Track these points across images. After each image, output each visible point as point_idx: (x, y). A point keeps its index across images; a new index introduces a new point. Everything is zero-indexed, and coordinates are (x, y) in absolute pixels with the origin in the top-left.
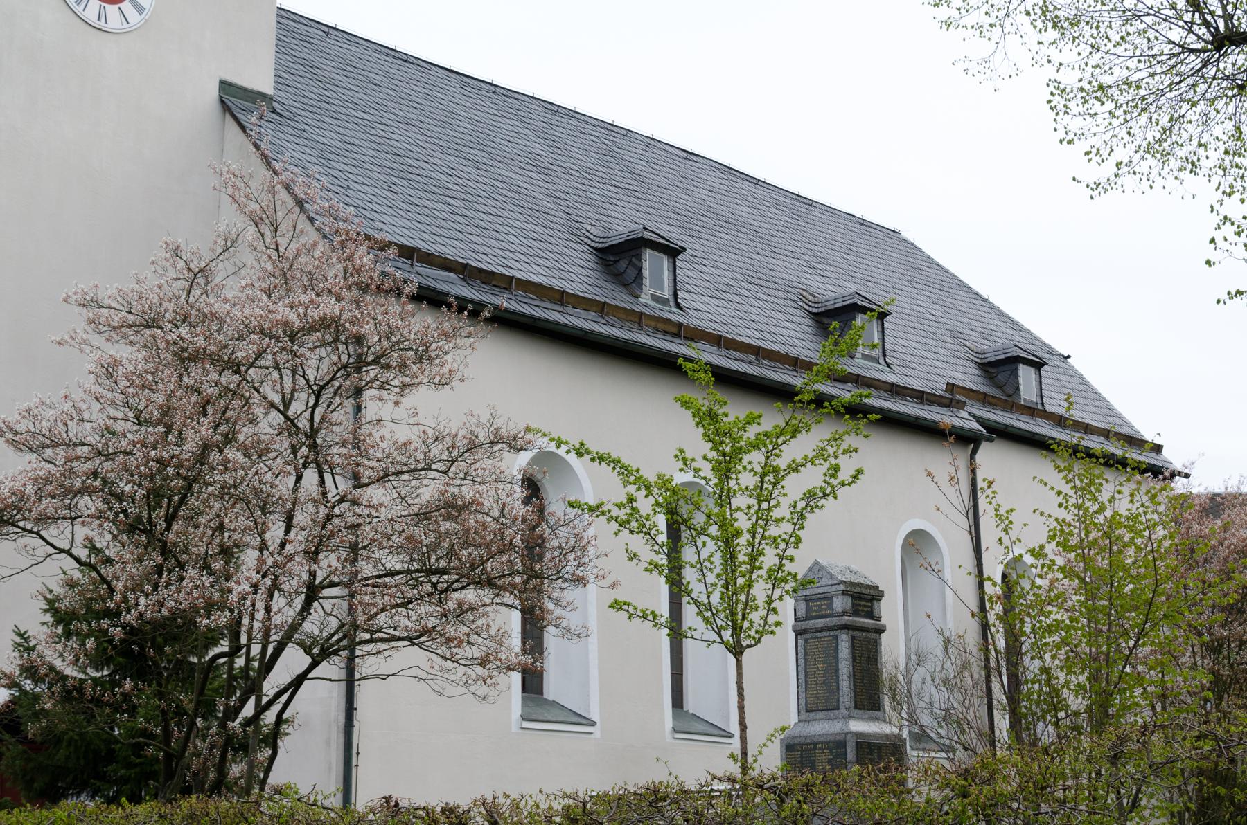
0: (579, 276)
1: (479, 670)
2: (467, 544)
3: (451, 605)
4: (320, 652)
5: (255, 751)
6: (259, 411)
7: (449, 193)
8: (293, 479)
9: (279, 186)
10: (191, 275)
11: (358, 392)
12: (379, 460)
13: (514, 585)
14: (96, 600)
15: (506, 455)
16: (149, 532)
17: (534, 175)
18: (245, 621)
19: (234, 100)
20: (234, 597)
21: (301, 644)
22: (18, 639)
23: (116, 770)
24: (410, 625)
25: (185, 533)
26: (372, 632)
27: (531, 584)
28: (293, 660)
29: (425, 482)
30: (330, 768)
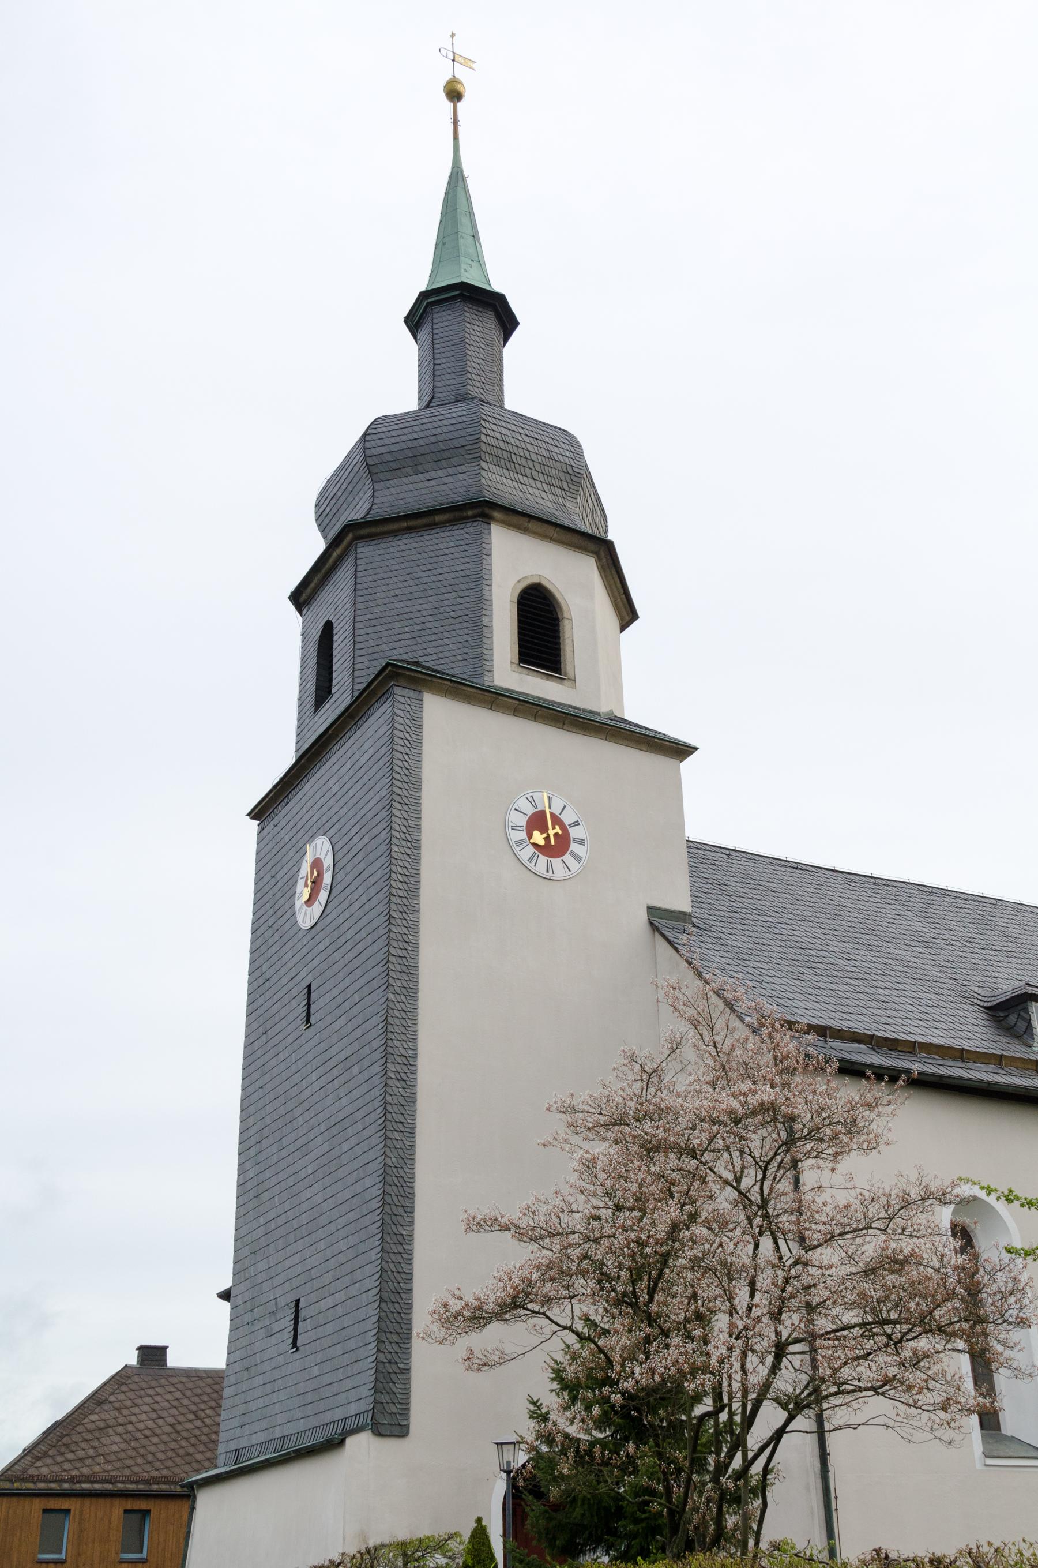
0: (974, 1033)
1: (942, 1414)
2: (912, 1296)
3: (907, 1354)
4: (794, 1406)
5: (747, 1504)
6: (716, 1188)
7: (849, 975)
8: (751, 1247)
9: (711, 993)
10: (645, 1077)
11: (795, 1163)
12: (824, 1224)
13: (963, 1331)
14: (595, 1369)
15: (937, 1208)
16: (634, 1305)
17: (920, 950)
18: (725, 1384)
19: (662, 922)
20: (713, 1361)
21: (777, 1400)
22: (532, 1408)
23: (625, 1526)
24: (872, 1375)
25: (665, 1303)
26: (839, 1385)
27: (979, 1328)
28: (770, 1417)
29: (868, 1239)
30: (812, 1513)
